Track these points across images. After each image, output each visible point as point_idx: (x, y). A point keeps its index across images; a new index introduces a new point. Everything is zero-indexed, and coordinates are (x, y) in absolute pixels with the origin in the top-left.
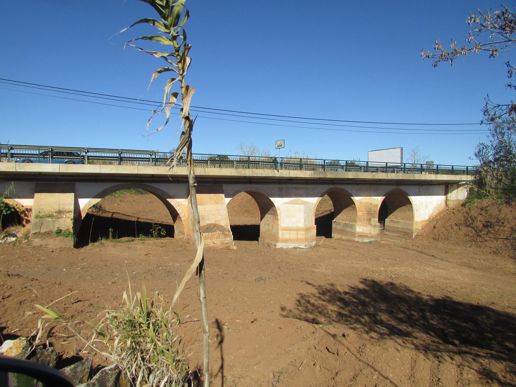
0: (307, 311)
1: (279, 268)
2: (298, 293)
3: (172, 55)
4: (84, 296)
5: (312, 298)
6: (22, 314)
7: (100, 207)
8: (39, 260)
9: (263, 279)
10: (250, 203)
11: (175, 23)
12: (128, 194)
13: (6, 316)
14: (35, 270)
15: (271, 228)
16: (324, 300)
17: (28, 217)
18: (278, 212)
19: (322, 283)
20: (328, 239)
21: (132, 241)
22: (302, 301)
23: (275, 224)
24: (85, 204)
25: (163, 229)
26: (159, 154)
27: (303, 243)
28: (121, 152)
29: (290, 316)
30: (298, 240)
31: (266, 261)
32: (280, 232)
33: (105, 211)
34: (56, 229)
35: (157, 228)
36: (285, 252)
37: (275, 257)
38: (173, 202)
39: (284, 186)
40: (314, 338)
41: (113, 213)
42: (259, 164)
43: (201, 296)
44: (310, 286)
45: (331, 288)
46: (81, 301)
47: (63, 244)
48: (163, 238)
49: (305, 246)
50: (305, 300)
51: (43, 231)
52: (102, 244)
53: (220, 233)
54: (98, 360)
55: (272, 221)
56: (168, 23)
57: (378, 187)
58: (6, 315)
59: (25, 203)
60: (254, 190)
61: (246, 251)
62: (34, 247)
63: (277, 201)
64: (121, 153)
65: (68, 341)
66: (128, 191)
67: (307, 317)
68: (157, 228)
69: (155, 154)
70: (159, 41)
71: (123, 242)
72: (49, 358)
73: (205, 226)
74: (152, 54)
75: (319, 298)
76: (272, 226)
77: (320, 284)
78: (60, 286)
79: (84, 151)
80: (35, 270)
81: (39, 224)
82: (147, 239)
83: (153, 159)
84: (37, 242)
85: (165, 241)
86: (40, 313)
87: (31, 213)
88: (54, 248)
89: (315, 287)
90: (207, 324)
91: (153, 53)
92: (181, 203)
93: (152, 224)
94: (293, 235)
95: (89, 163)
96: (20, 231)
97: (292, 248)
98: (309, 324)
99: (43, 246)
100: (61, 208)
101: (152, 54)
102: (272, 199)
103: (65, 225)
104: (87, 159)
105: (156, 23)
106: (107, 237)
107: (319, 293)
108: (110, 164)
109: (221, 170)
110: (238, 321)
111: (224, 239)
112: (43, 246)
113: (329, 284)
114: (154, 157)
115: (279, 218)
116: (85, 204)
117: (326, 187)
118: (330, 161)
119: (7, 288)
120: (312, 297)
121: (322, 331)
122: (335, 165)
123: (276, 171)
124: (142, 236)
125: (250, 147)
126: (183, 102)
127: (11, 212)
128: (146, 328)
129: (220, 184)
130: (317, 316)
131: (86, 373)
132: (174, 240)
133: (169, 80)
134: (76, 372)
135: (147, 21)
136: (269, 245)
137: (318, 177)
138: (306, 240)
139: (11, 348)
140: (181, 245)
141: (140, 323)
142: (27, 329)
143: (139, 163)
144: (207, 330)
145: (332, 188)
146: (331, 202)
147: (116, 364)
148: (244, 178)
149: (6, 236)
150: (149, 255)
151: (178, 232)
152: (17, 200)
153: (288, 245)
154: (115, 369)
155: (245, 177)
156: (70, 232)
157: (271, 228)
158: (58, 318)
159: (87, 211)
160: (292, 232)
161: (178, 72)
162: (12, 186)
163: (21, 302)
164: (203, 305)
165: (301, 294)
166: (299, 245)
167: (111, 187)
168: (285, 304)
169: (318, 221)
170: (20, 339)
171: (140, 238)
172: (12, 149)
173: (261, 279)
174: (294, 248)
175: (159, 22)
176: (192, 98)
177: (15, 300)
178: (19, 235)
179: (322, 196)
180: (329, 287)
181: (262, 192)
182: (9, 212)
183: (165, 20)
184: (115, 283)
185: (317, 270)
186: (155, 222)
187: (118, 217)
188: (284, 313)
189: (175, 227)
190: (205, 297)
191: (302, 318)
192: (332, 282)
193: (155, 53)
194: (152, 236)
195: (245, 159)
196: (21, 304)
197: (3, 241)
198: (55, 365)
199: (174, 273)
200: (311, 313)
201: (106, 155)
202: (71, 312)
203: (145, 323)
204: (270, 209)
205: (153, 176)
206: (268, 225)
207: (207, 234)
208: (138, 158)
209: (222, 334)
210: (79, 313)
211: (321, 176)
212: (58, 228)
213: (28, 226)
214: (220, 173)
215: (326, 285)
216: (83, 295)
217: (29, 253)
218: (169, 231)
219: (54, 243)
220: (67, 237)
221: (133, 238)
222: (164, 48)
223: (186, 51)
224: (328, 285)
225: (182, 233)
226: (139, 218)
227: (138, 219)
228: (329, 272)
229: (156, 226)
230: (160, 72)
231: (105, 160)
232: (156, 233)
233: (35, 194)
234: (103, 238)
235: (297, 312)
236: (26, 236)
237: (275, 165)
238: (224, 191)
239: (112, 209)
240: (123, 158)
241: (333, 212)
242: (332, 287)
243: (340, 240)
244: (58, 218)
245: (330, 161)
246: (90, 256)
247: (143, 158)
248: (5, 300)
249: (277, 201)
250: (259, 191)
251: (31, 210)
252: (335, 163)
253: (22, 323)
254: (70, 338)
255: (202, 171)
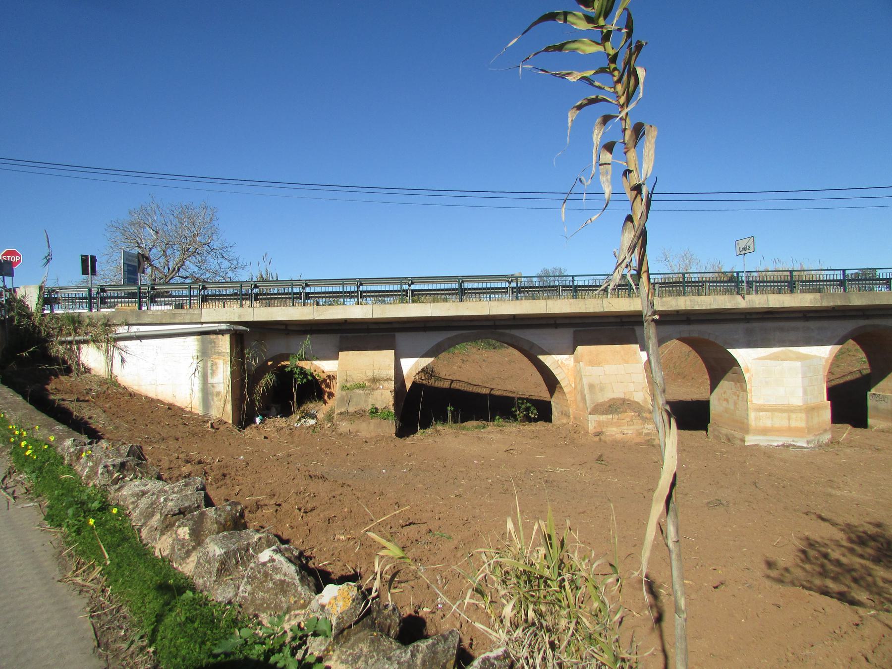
0: (824, 574)
1: (755, 483)
2: (801, 535)
3: (602, 70)
4: (418, 516)
5: (833, 550)
6: (332, 538)
7: (432, 371)
8: (348, 455)
9: (722, 504)
10: (686, 359)
11: (608, 8)
12: (474, 350)
13: (311, 540)
14: (344, 470)
15: (732, 408)
16: (862, 556)
17: (330, 388)
18: (747, 376)
19: (854, 521)
20: (859, 431)
21: (484, 427)
22: (812, 553)
23: (740, 398)
24: (411, 366)
25: (532, 408)
26: (523, 279)
27: (802, 437)
28: (461, 280)
29: (787, 580)
30: (790, 430)
31: (727, 469)
32: (752, 415)
33: (439, 379)
34: (370, 407)
35: (523, 406)
36: (765, 453)
37: (745, 462)
38: (548, 360)
39: (756, 325)
40: (860, 636)
41: (452, 381)
42: (704, 286)
43: (669, 538)
44: (827, 524)
45: (877, 532)
46: (414, 524)
47: (380, 430)
48: (533, 423)
49: (808, 442)
50: (819, 551)
51: (351, 410)
52: (437, 431)
53: (634, 415)
54: (448, 626)
55: (735, 394)
56: (593, 10)
58: (309, 538)
59: (325, 367)
60: (695, 335)
61: (684, 450)
62: (341, 434)
63: (742, 355)
64: (463, 282)
65: (400, 588)
66: (474, 344)
67: (826, 587)
68: (523, 406)
69: (517, 279)
70: (577, 49)
71: (469, 429)
72: (389, 621)
73: (607, 402)
74: (563, 77)
75: (852, 551)
76: (735, 404)
77: (849, 522)
78: (382, 497)
79: (406, 282)
80: (344, 470)
81: (346, 398)
82: (507, 424)
83: (513, 288)
84: (344, 426)
85: (538, 428)
86: (357, 539)
87: (334, 383)
88: (367, 436)
89: (839, 527)
90: (682, 594)
91: (564, 75)
92: (562, 363)
93: (513, 398)
94: (780, 421)
95: (413, 302)
96: (321, 410)
97: (778, 446)
98: (840, 605)
99: (352, 433)
100: (376, 373)
101: (563, 77)
102: (732, 351)
103: (382, 401)
104: (411, 294)
105: (570, 18)
106: (444, 420)
107: (850, 540)
108: (445, 300)
109: (631, 300)
110: (687, 582)
111: (641, 427)
112: (352, 433)
113: (870, 523)
114: (515, 286)
115: (748, 387)
116: (411, 366)
117: (851, 325)
118: (854, 272)
119: (309, 496)
120: (834, 547)
121: (879, 625)
122: (866, 280)
123: (739, 298)
124: (499, 419)
125: (683, 258)
126: (627, 159)
127: (308, 380)
128: (558, 589)
129: (631, 327)
130: (849, 587)
131: (450, 655)
132: (553, 427)
133: (599, 120)
134: (435, 653)
135: (552, 16)
136: (729, 440)
137: (832, 304)
138: (809, 430)
139: (335, 598)
140: (564, 435)
141: (547, 578)
142: (340, 564)
143: (490, 297)
144: (683, 607)
146: (862, 355)
147: (505, 648)
148: (675, 313)
149: (303, 417)
150: (511, 451)
151: (558, 413)
152: (317, 363)
153: (769, 441)
154: (505, 658)
155: (678, 311)
156: (389, 412)
157: (732, 407)
158: (403, 558)
159: (413, 379)
160: (776, 413)
161: (616, 103)
162: (307, 342)
163: (329, 520)
164: (674, 556)
165: (807, 539)
166: (793, 441)
167: (449, 338)
168: (772, 557)
169: (834, 393)
170: (348, 584)
171: (496, 423)
172: (307, 285)
173: (719, 503)
174: (783, 445)
175: (575, 15)
176: (657, 143)
177: (322, 516)
178: (320, 416)
179: (841, 342)
180: (872, 530)
181: (712, 339)
182: (305, 380)
183: (587, 6)
184: (461, 496)
185: (838, 493)
186: (518, 396)
187: (460, 388)
188: (774, 573)
189: (553, 404)
190: (678, 541)
191: (814, 588)
192: (879, 520)
193: (568, 74)
194: (516, 420)
195: (674, 278)
196: (329, 523)
197: (299, 425)
198: (398, 633)
199: (555, 484)
200: (835, 579)
201: (438, 286)
202: (401, 541)
203: (555, 579)
204: (729, 370)
205: (514, 317)
206: (726, 400)
207: (610, 416)
208: (489, 289)
209: (659, 604)
210: (412, 543)
211: (839, 303)
212: (373, 405)
213: (331, 403)
214: (630, 306)
215: (865, 524)
216: (416, 514)
217: (334, 443)
218: (543, 411)
219: (367, 429)
220: (385, 419)
221: (484, 422)
222: (585, 61)
223: (634, 57)
224: (868, 525)
225: (565, 414)
226: (492, 389)
227: (491, 390)
228: (867, 498)
229: (521, 402)
230: (579, 107)
231: (436, 295)
232: (521, 415)
233: (340, 353)
234: (438, 421)
235: (799, 573)
236: (330, 418)
237: (737, 286)
238: (639, 341)
239: (449, 375)
240: (466, 289)
241: (868, 375)
242: (879, 531)
243: (888, 432)
244: (373, 390)
245: (857, 271)
246: (421, 451)
247: (496, 288)
248: (308, 514)
249: (742, 355)
250: (706, 337)
251: (334, 378)
252: (866, 274)
253: (332, 553)
254: (403, 585)
255: (598, 304)
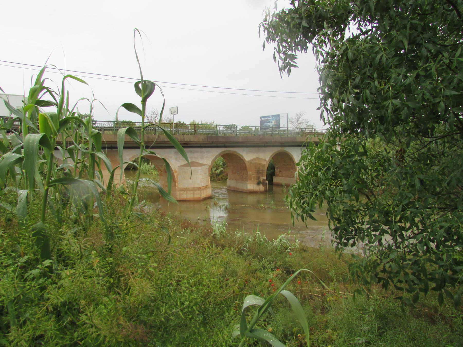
18: (175, 175)
57: (265, 148)
145: (224, 151)
